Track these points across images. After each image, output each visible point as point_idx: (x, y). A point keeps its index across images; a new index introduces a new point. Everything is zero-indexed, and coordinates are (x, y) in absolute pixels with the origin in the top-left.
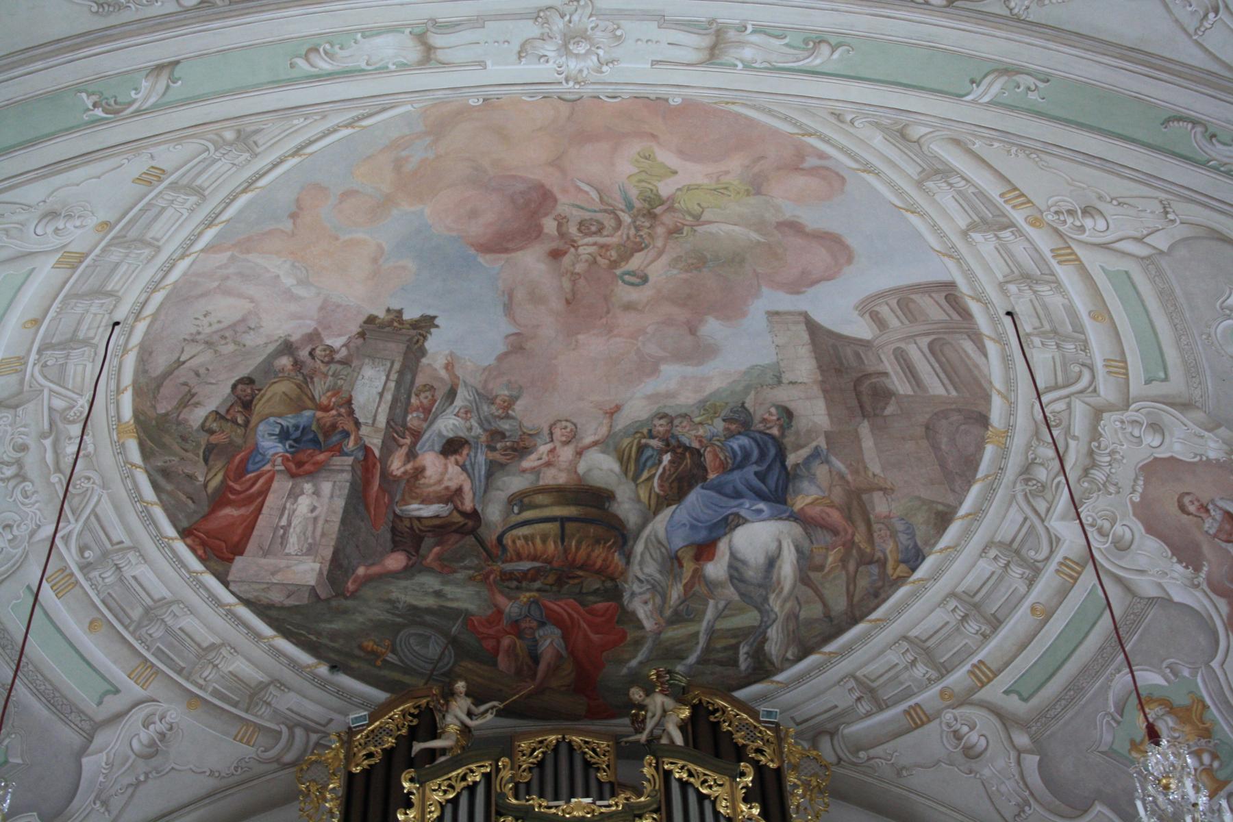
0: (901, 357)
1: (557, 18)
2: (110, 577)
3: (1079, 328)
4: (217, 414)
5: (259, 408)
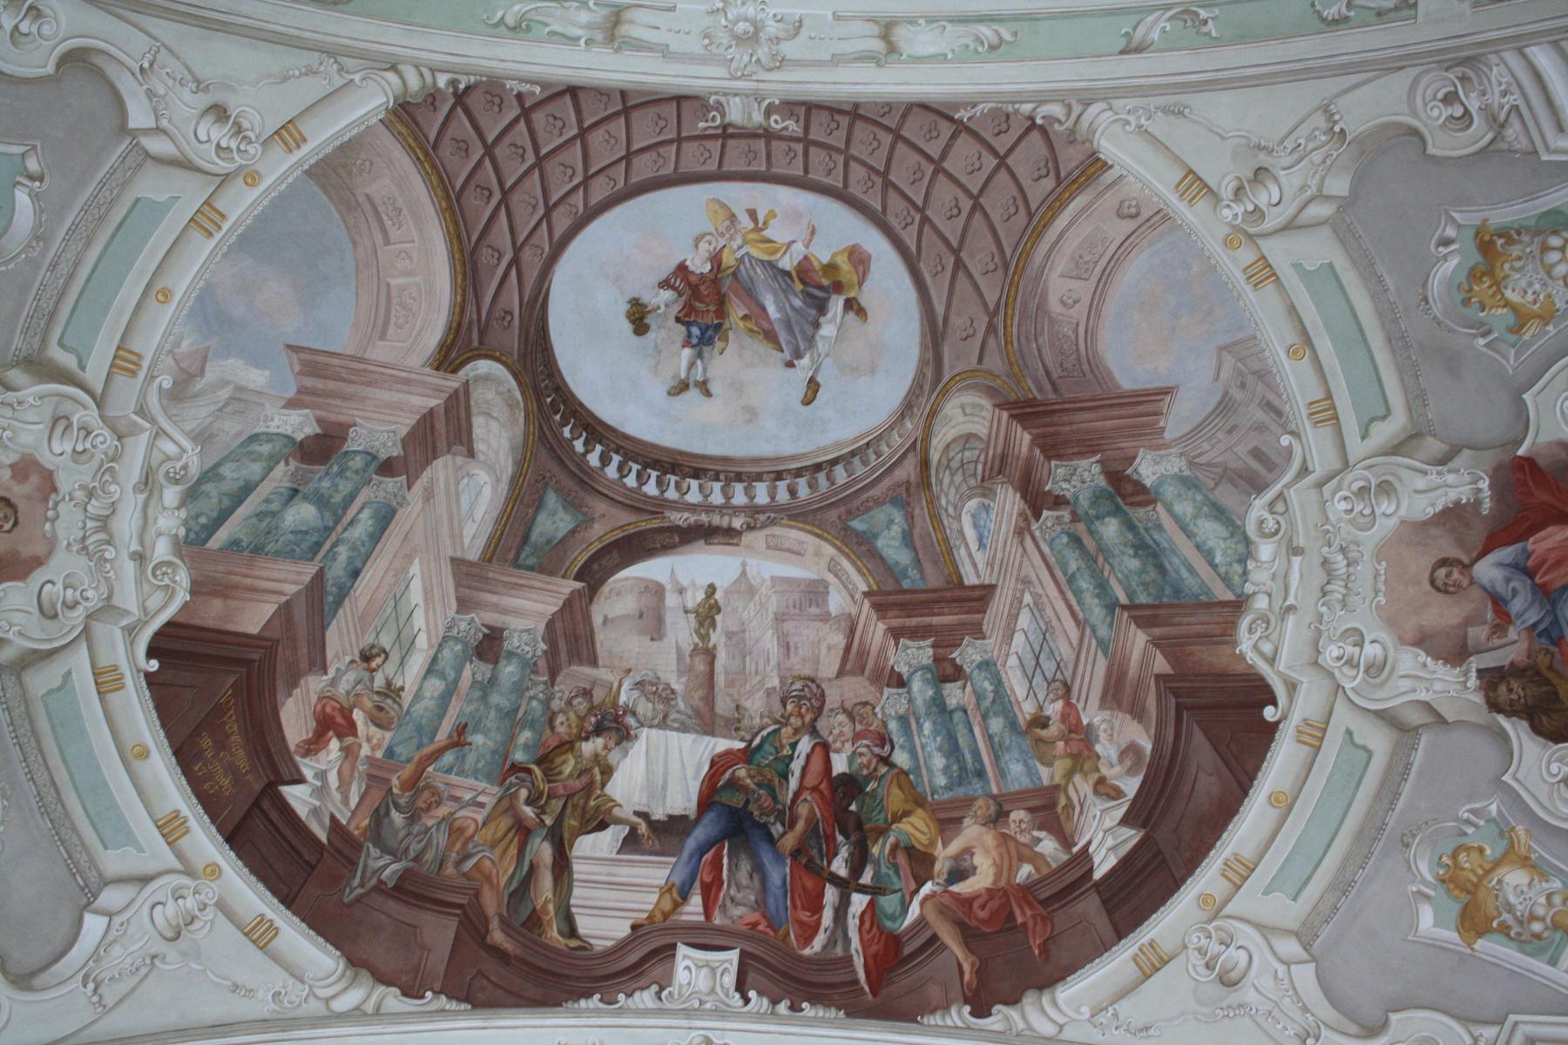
1: (764, 61)
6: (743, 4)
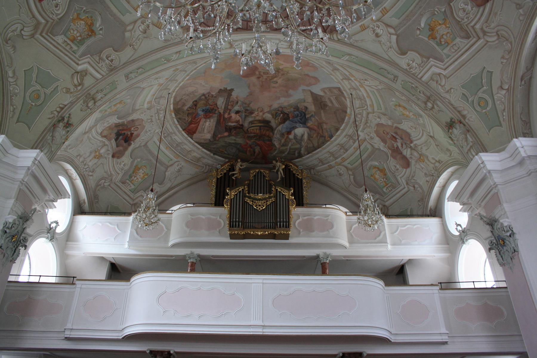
0: (330, 99)
2: (169, 139)
3: (364, 98)
4: (190, 107)
5: (198, 106)
6: (286, 1)
